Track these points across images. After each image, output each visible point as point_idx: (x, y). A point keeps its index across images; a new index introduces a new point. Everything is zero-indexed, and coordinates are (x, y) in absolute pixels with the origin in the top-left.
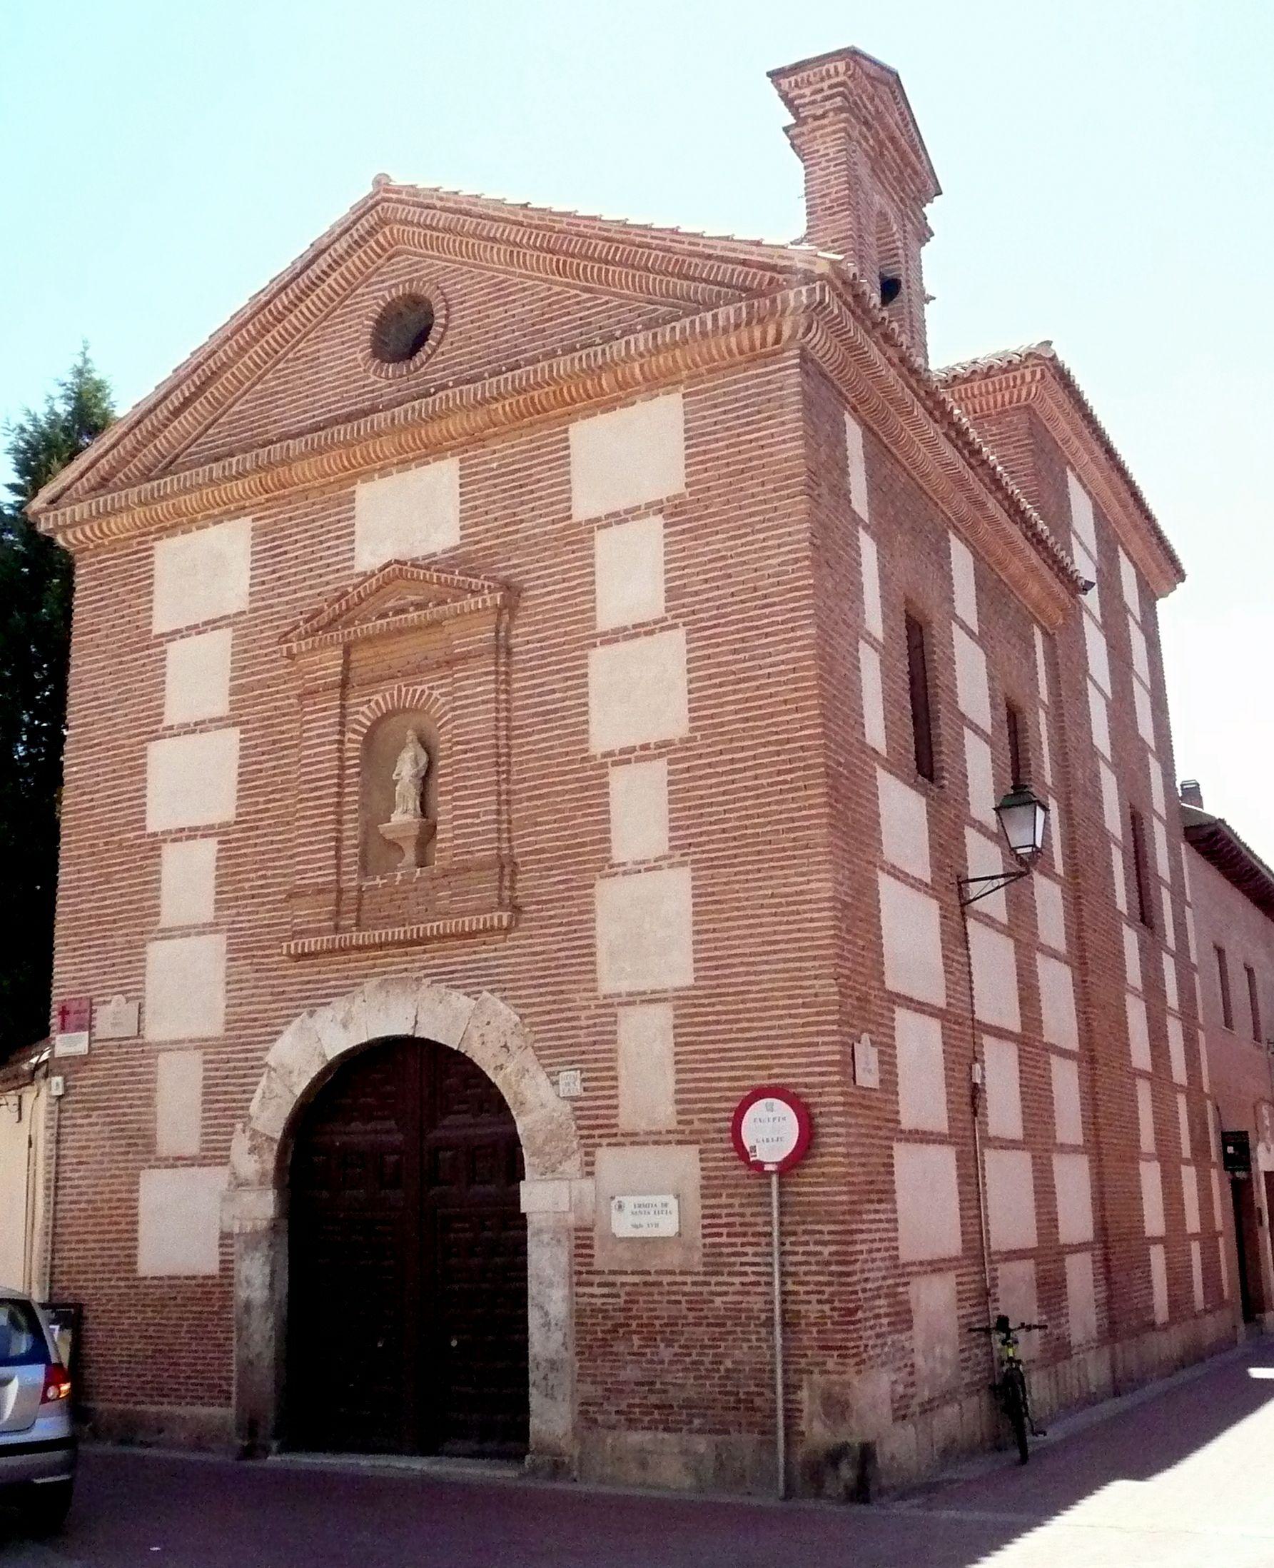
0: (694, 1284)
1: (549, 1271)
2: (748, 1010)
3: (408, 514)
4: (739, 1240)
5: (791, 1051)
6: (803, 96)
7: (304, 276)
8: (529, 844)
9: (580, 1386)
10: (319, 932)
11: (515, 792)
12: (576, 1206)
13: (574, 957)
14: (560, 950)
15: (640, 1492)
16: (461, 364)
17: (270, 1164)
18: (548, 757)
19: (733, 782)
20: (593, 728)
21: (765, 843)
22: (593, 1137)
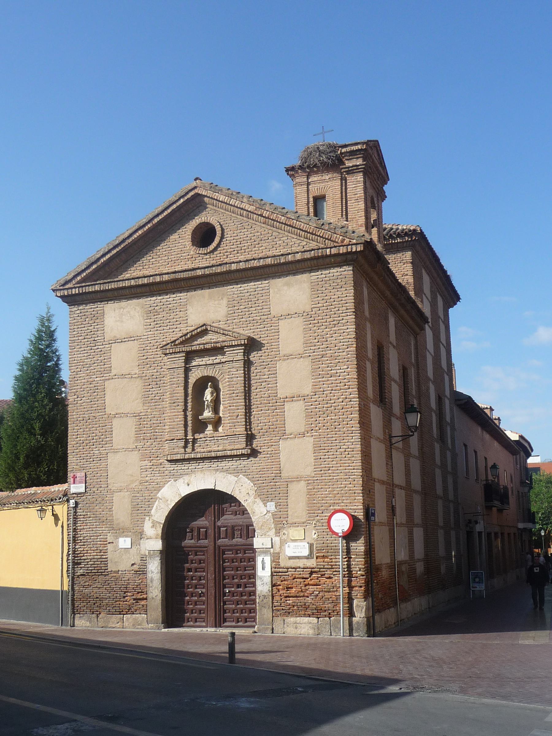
17: (160, 531)
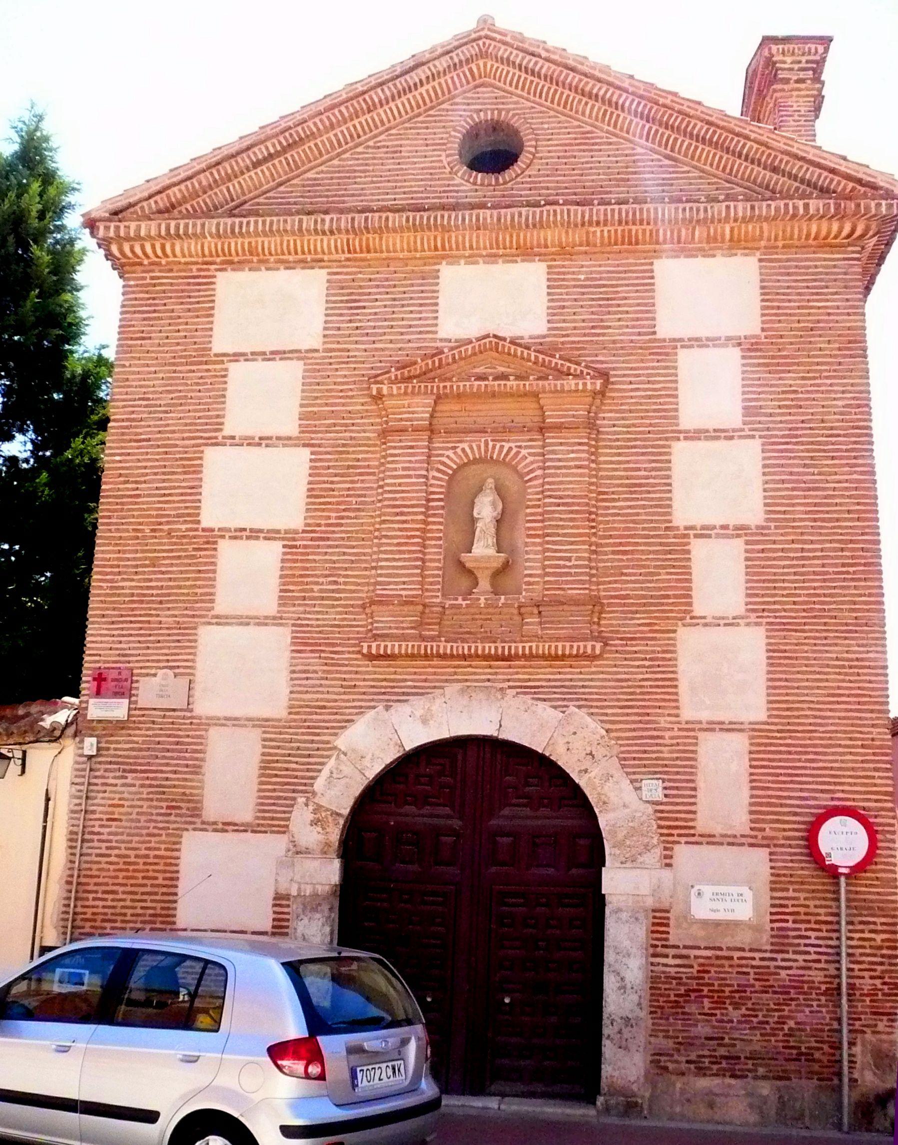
0: (762, 959)
1: (627, 943)
2: (815, 746)
3: (491, 299)
4: (803, 926)
5: (850, 780)
6: (785, 62)
7: (402, 79)
8: (615, 589)
9: (652, 1039)
10: (404, 638)
11: (601, 545)
12: (656, 890)
13: (658, 687)
14: (643, 680)
15: (710, 1127)
16: (548, 188)
17: (335, 834)
18: (634, 522)
19: (803, 566)
20: (676, 504)
21: (831, 617)
22: (673, 835)
